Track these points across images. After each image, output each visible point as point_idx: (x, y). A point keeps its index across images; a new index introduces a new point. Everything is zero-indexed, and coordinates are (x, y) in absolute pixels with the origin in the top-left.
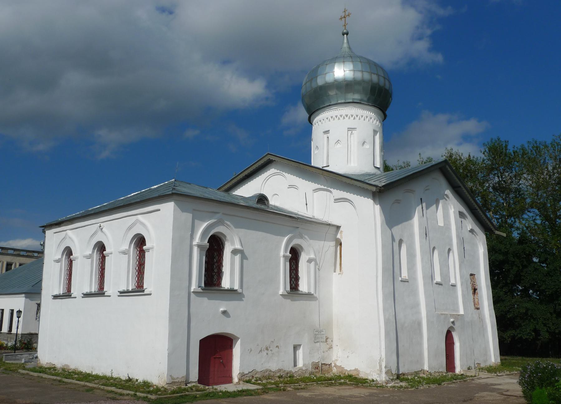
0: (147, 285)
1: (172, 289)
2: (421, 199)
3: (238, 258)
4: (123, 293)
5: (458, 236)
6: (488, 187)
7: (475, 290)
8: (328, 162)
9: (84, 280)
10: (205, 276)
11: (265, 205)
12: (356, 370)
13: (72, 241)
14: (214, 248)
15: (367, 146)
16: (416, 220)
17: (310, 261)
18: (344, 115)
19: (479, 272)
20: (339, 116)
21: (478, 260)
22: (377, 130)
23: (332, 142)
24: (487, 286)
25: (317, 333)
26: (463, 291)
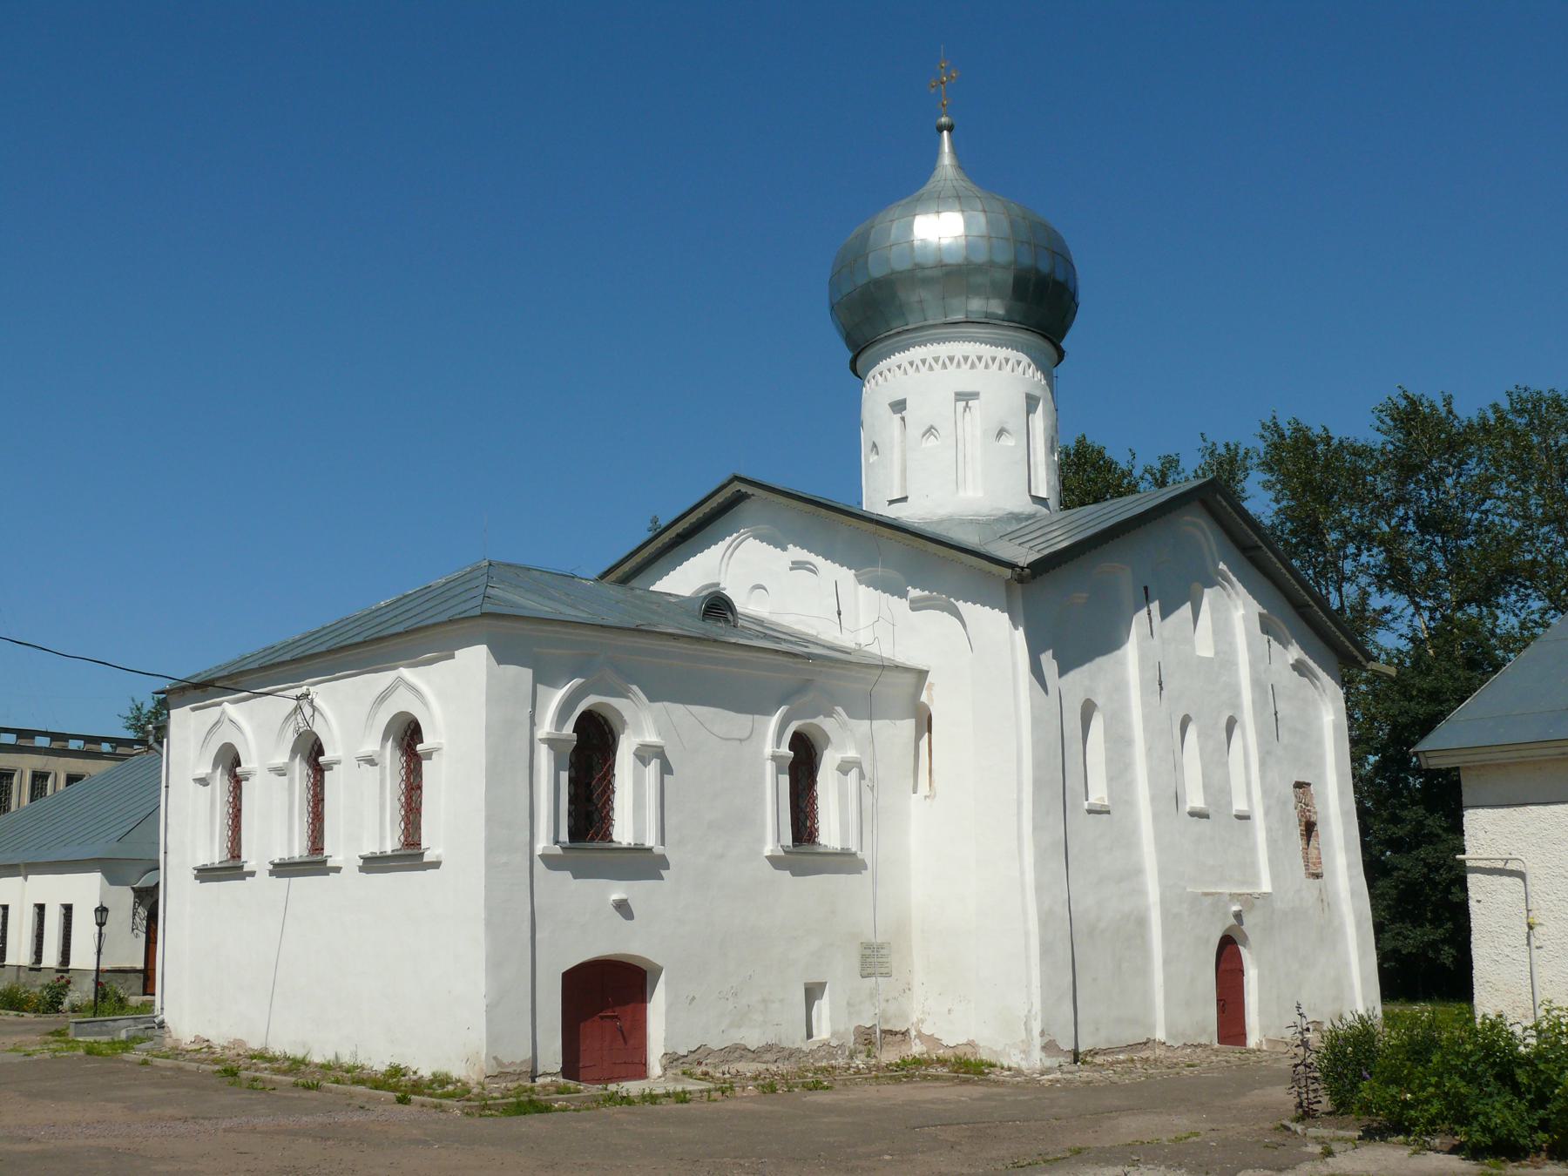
0: (433, 843)
1: (490, 850)
2: (1146, 588)
3: (653, 767)
4: (372, 864)
5: (1256, 683)
6: (1405, 519)
7: (1309, 829)
8: (904, 487)
9: (274, 829)
10: (570, 814)
11: (727, 620)
12: (970, 1044)
13: (239, 728)
14: (590, 753)
15: (1008, 441)
16: (1131, 651)
17: (844, 768)
18: (943, 357)
19: (1321, 777)
20: (930, 360)
21: (1320, 743)
22: (1037, 393)
23: (914, 431)
24: (1344, 813)
25: (868, 952)
26: (1269, 830)
